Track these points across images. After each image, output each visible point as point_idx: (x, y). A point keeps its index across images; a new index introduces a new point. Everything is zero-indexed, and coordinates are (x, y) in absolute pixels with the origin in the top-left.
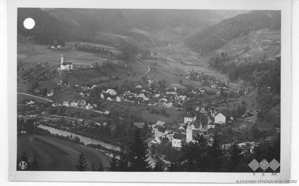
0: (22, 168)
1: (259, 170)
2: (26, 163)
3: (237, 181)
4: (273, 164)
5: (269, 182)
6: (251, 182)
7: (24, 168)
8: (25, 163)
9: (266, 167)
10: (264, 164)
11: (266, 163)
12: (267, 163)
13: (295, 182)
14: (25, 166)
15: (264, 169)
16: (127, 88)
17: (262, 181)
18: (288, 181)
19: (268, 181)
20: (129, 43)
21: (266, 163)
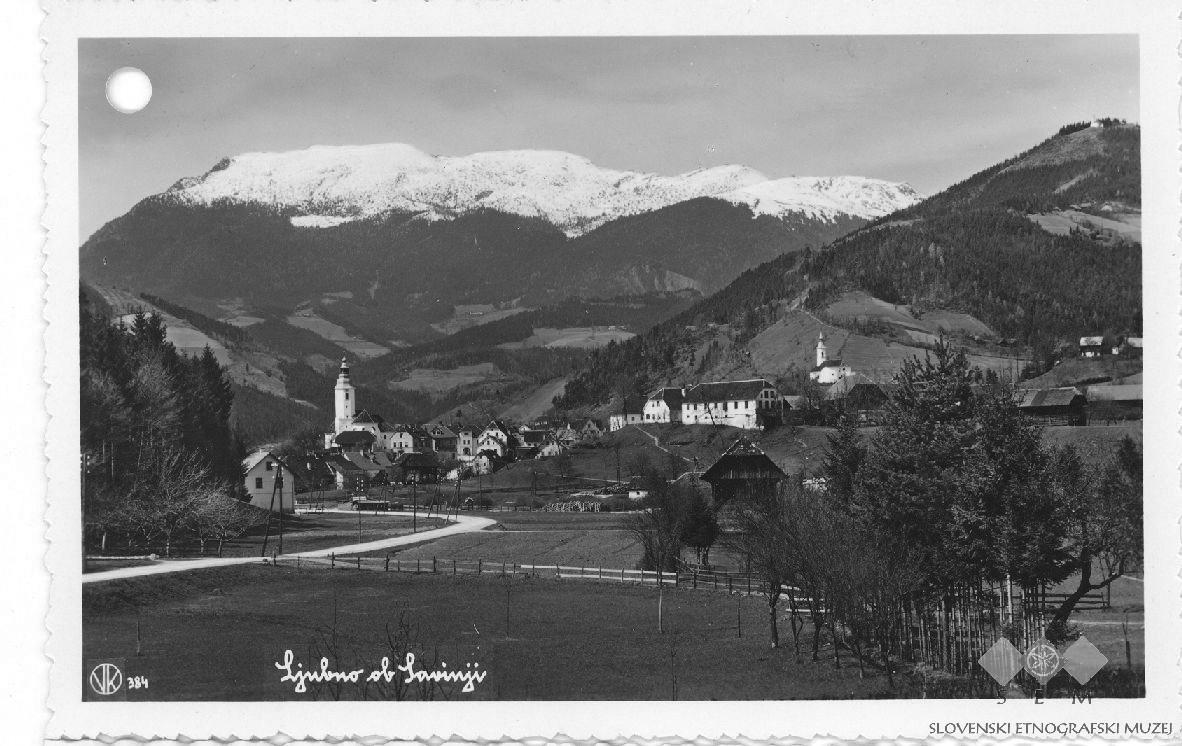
0: (103, 689)
1: (1030, 687)
2: (118, 671)
3: (933, 726)
4: (1085, 658)
6: (990, 730)
7: (111, 690)
14: (116, 683)
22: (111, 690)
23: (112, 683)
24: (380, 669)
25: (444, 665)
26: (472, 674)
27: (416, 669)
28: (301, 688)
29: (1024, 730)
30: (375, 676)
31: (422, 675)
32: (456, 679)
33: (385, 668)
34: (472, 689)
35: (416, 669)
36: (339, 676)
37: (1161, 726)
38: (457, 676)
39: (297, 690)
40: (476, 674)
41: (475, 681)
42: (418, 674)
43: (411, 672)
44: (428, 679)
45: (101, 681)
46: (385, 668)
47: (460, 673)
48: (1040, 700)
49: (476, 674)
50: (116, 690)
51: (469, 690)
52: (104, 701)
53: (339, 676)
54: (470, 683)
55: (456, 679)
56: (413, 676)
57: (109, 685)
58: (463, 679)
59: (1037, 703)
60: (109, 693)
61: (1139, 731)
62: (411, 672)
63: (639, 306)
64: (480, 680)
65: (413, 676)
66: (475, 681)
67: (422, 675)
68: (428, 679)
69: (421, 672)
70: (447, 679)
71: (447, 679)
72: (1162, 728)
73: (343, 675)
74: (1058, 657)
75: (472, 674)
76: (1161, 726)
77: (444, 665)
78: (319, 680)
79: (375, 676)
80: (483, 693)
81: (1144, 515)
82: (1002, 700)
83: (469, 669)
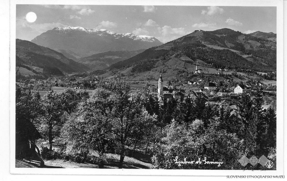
0: (269, 167)
1: (249, 167)
2: (272, 163)
3: (227, 176)
4: (263, 160)
5: (256, 177)
6: (241, 177)
7: (271, 167)
8: (271, 162)
9: (255, 163)
10: (254, 160)
11: (255, 158)
12: (256, 159)
13: (284, 177)
14: (272, 165)
15: (244, 165)
16: (80, 143)
17: (252, 176)
18: (276, 176)
19: (257, 178)
20: (202, 84)
21: (255, 158)
22: (271, 167)
23: (271, 165)
24: (198, 161)
25: (213, 160)
26: (220, 162)
27: (207, 161)
28: (180, 165)
29: (249, 177)
30: (197, 162)
31: (208, 162)
32: (216, 163)
33: (199, 160)
34: (220, 166)
35: (207, 161)
36: (188, 162)
37: (282, 176)
38: (216, 163)
39: (179, 166)
40: (221, 162)
41: (221, 164)
42: (207, 162)
43: (206, 162)
44: (210, 163)
45: (268, 165)
46: (199, 160)
47: (217, 162)
48: (253, 170)
49: (221, 162)
50: (272, 167)
51: (219, 166)
52: (133, 168)
53: (188, 162)
54: (219, 164)
55: (216, 163)
56: (206, 163)
57: (270, 166)
58: (218, 163)
59: (252, 171)
60: (270, 168)
61: (277, 177)
62: (206, 162)
63: (265, 64)
64: (222, 164)
65: (206, 163)
66: (221, 164)
67: (208, 162)
68: (210, 163)
69: (208, 162)
70: (214, 163)
71: (214, 163)
72: (282, 177)
73: (189, 162)
74: (257, 160)
75: (220, 162)
76: (282, 176)
77: (213, 160)
78: (184, 163)
79: (197, 162)
80: (222, 168)
81: (15, 97)
82: (244, 170)
83: (219, 161)
